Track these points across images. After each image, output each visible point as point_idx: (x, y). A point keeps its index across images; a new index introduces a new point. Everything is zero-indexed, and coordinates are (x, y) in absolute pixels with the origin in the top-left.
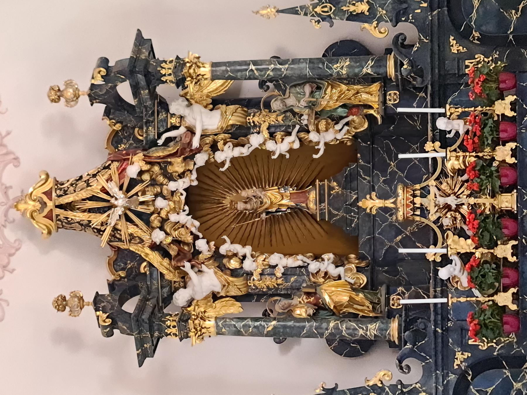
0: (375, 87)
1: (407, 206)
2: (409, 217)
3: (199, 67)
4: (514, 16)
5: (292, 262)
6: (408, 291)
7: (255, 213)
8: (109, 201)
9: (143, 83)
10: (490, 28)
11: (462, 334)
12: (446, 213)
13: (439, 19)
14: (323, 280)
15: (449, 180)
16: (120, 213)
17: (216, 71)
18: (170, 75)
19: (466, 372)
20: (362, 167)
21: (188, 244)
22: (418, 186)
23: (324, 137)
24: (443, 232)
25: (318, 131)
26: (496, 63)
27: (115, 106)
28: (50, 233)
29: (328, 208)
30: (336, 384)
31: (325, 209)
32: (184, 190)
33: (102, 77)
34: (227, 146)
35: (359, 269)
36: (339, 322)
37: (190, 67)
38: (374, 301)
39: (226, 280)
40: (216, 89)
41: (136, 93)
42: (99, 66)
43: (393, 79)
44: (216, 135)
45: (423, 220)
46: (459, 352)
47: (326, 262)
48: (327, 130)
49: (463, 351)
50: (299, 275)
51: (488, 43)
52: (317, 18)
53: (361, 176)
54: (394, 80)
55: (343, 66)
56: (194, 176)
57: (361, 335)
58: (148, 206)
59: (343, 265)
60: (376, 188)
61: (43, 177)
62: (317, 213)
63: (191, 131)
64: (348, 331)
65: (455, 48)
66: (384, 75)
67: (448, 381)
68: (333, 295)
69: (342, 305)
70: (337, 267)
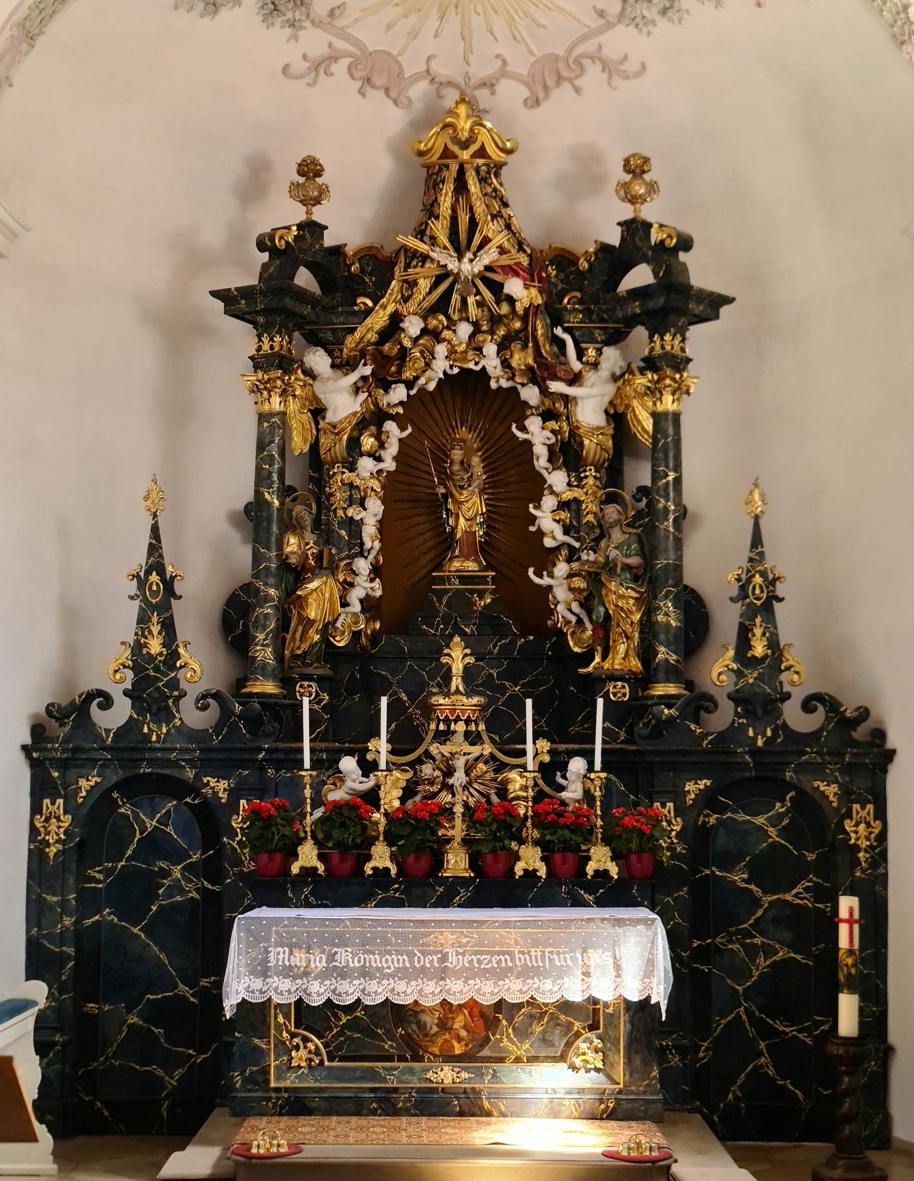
0: (635, 664)
3: (673, 394)
4: (739, 877)
5: (369, 531)
6: (322, 708)
7: (445, 477)
9: (651, 305)
10: (722, 841)
12: (440, 770)
14: (341, 580)
16: (450, 267)
17: (666, 419)
18: (663, 347)
19: (198, 794)
21: (399, 372)
22: (482, 727)
23: (560, 584)
24: (412, 764)
25: (570, 576)
27: (614, 261)
28: (421, 154)
29: (452, 589)
30: (180, 597)
32: (484, 368)
33: (662, 241)
34: (550, 435)
37: (674, 379)
39: (343, 430)
44: (568, 418)
45: (431, 735)
48: (571, 589)
51: (698, 838)
52: (744, 577)
55: (668, 615)
56: (505, 384)
57: (257, 637)
58: (460, 311)
59: (363, 610)
63: (575, 379)
65: (693, 788)
67: (184, 767)
68: (318, 595)
69: (302, 608)
70: (361, 601)
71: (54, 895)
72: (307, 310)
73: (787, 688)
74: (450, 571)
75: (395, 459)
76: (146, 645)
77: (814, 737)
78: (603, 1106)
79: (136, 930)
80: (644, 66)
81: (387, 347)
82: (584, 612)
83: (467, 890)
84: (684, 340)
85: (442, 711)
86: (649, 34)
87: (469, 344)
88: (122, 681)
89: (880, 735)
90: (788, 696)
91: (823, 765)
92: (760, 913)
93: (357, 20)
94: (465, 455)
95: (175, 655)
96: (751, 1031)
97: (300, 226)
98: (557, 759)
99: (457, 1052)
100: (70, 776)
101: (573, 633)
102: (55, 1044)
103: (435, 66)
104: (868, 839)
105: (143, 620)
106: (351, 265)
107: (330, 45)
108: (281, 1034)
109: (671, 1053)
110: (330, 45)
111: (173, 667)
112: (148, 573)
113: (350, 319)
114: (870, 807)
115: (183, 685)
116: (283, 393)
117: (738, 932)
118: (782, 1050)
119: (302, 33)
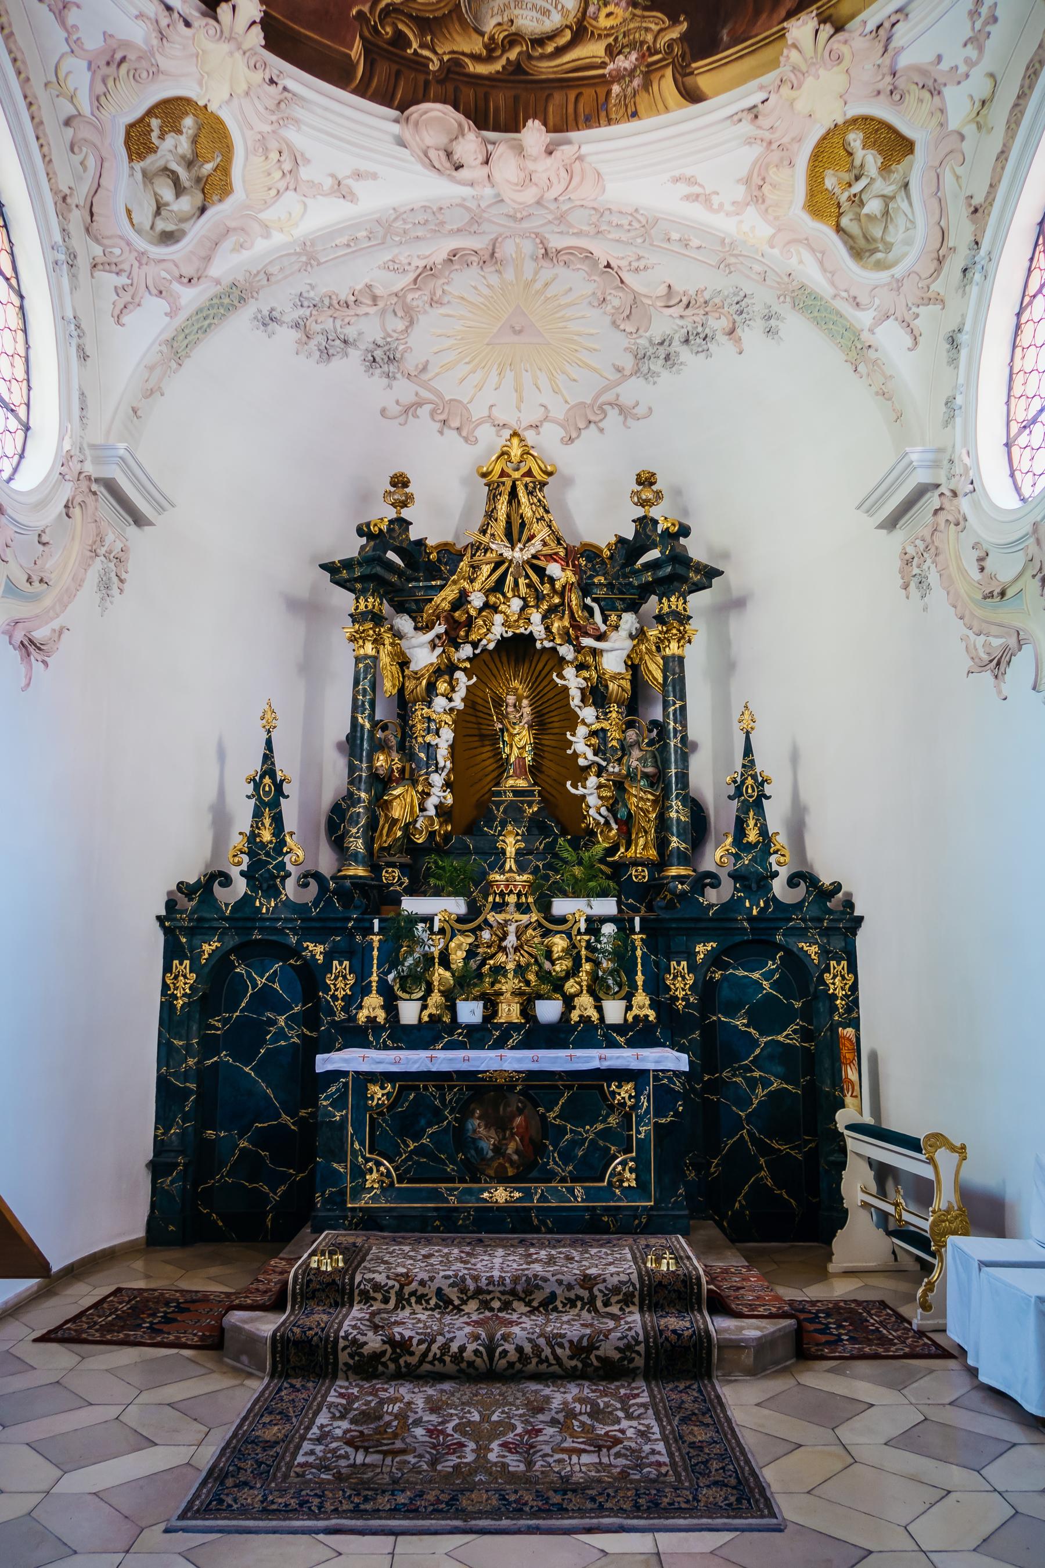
0: (652, 853)
1: (507, 886)
3: (679, 642)
4: (740, 1022)
5: (442, 754)
6: (404, 890)
7: (503, 717)
8: (519, 541)
9: (661, 574)
10: (726, 993)
12: (497, 935)
13: (738, 929)
16: (505, 555)
17: (674, 661)
18: (670, 607)
19: (300, 957)
20: (555, 841)
21: (467, 636)
22: (530, 900)
23: (591, 793)
24: (473, 931)
25: (600, 786)
26: (683, 999)
27: (629, 550)
28: (484, 475)
30: (288, 797)
32: (531, 632)
33: (668, 528)
34: (583, 681)
37: (679, 630)
39: (423, 675)
40: (650, 671)
41: (648, 566)
42: (680, 524)
44: (596, 668)
45: (489, 906)
47: (442, 794)
48: (600, 798)
49: (325, 954)
50: (427, 763)
51: (706, 990)
52: (739, 780)
53: (544, 839)
55: (677, 812)
56: (548, 644)
58: (513, 590)
59: (437, 815)
61: (549, 468)
63: (601, 637)
65: (702, 949)
67: (288, 935)
68: (401, 802)
69: (388, 809)
70: (436, 807)
71: (180, 1040)
72: (394, 579)
73: (775, 867)
75: (463, 700)
76: (259, 835)
77: (798, 906)
78: (637, 1222)
79: (247, 1070)
80: (650, 409)
81: (457, 614)
83: (519, 1034)
84: (685, 603)
85: (498, 886)
86: (655, 383)
87: (520, 615)
88: (239, 864)
89: (849, 904)
90: (776, 874)
91: (807, 929)
92: (758, 1051)
93: (438, 374)
94: (517, 700)
95: (283, 843)
96: (753, 1150)
97: (391, 522)
98: (591, 926)
99: (510, 1174)
100: (196, 941)
101: (602, 832)
102: (178, 1164)
103: (495, 412)
104: (843, 989)
105: (257, 814)
106: (431, 553)
107: (417, 394)
108: (357, 1160)
109: (688, 1169)
110: (417, 394)
111: (280, 853)
112: (262, 777)
113: (429, 592)
114: (844, 963)
115: (289, 867)
116: (375, 642)
117: (741, 1067)
118: (779, 1164)
119: (395, 383)
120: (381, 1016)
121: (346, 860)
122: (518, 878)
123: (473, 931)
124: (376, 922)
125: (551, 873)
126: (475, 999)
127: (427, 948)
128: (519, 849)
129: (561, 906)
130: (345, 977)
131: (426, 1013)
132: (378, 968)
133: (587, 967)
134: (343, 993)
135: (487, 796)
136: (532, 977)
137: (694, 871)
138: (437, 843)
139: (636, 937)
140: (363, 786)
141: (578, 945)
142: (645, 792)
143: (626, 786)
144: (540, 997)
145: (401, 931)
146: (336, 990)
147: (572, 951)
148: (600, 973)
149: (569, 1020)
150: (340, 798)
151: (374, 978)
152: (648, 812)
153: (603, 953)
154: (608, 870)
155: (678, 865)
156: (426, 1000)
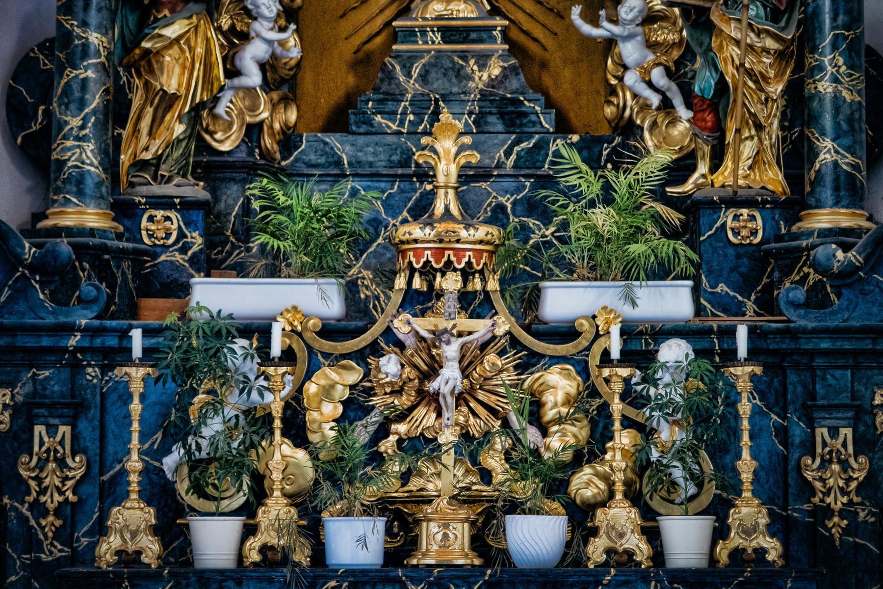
0: (773, 178)
2: (404, 258)
11: (65, 405)
12: (415, 366)
14: (225, 27)
15: (509, 377)
20: (541, 146)
22: (493, 285)
24: (360, 356)
26: (842, 514)
29: (429, 51)
31: (426, 43)
35: (256, 131)
36: (103, 59)
38: (163, 167)
43: (798, 224)
45: (397, 298)
46: (13, 397)
47: (274, 36)
48: (651, 46)
53: (517, 142)
54: (794, 229)
57: (66, 123)
59: (267, 85)
60: (484, 185)
62: (416, 19)
64: (76, 87)
66: (812, 201)
69: (151, 71)
70: (263, 67)
74: (427, 19)
82: (674, 87)
85: (418, 253)
98: (634, 346)
101: (654, 125)
120: (151, 548)
121: (58, 191)
122: (463, 234)
123: (360, 356)
124: (137, 335)
125: (531, 222)
126: (367, 511)
127: (255, 395)
128: (467, 166)
129: (562, 300)
130: (61, 463)
131: (254, 544)
132: (142, 441)
133: (624, 439)
134: (57, 498)
135: (378, 40)
136: (494, 462)
137: (870, 219)
138: (265, 154)
139: (739, 371)
140: (94, 17)
141: (603, 388)
142: (758, 34)
143: (715, 18)
144: (514, 507)
145: (194, 358)
146: (43, 491)
147: (590, 405)
148: (655, 455)
149: (580, 561)
150: (33, 43)
151: (134, 463)
152: (766, 79)
153: (661, 408)
154: (674, 216)
155: (837, 203)
156: (253, 515)
